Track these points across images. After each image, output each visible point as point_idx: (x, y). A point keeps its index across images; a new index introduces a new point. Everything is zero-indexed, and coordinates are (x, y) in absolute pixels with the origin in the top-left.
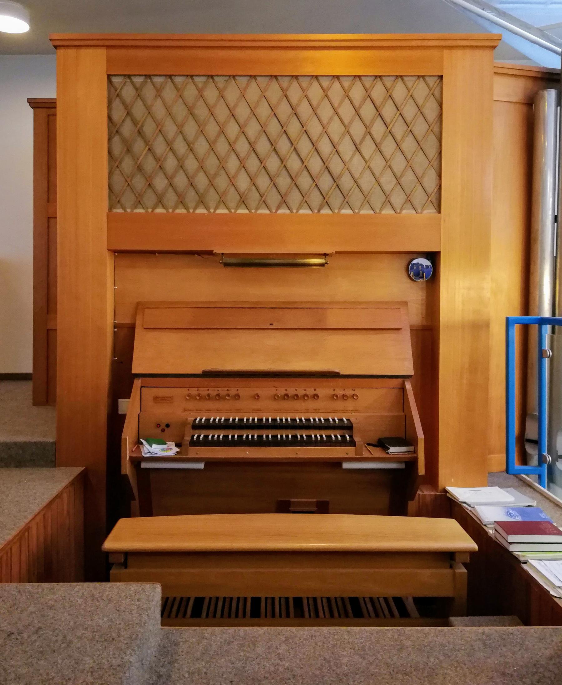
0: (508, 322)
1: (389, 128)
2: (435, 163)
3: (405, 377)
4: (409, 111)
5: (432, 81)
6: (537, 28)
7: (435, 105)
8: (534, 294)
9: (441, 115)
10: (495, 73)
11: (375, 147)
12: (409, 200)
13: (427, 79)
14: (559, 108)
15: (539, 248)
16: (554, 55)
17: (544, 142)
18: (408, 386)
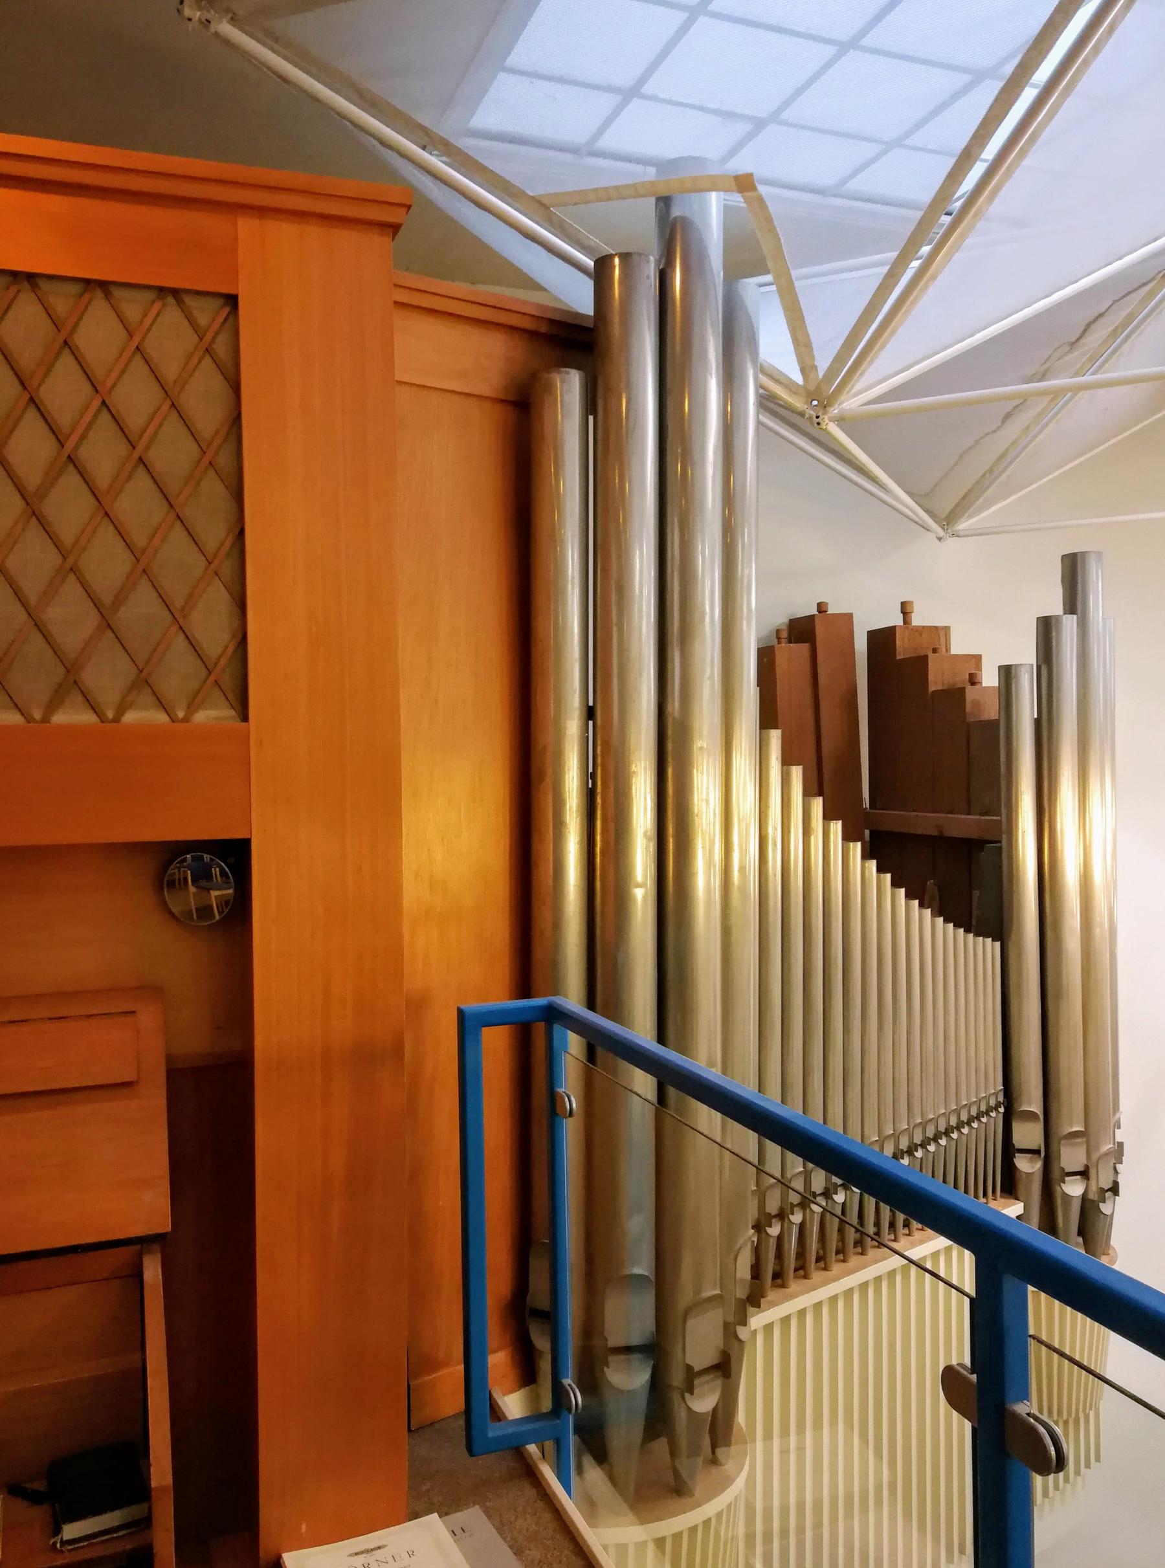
0: (467, 1026)
1: (69, 446)
2: (227, 568)
3: (144, 1242)
4: (136, 397)
5: (206, 313)
6: (533, 198)
7: (218, 384)
8: (544, 849)
9: (236, 420)
10: (396, 303)
11: (23, 503)
12: (142, 682)
13: (190, 301)
14: (591, 418)
15: (552, 695)
16: (624, 115)
17: (557, 482)
18: (152, 1271)
